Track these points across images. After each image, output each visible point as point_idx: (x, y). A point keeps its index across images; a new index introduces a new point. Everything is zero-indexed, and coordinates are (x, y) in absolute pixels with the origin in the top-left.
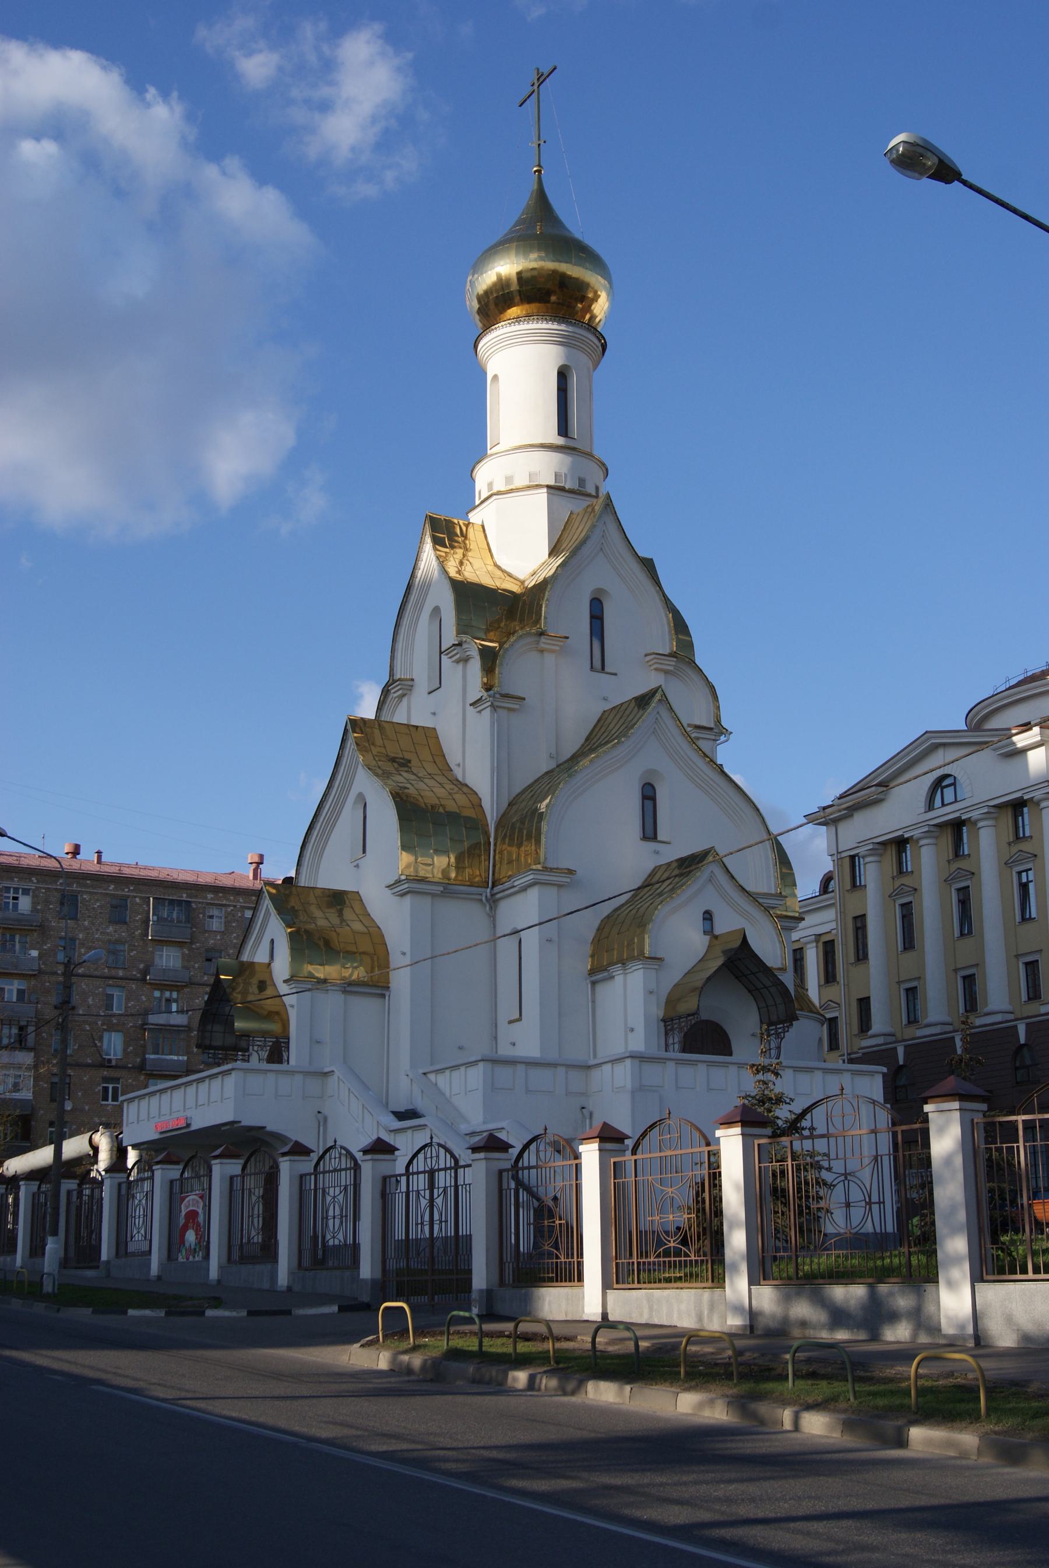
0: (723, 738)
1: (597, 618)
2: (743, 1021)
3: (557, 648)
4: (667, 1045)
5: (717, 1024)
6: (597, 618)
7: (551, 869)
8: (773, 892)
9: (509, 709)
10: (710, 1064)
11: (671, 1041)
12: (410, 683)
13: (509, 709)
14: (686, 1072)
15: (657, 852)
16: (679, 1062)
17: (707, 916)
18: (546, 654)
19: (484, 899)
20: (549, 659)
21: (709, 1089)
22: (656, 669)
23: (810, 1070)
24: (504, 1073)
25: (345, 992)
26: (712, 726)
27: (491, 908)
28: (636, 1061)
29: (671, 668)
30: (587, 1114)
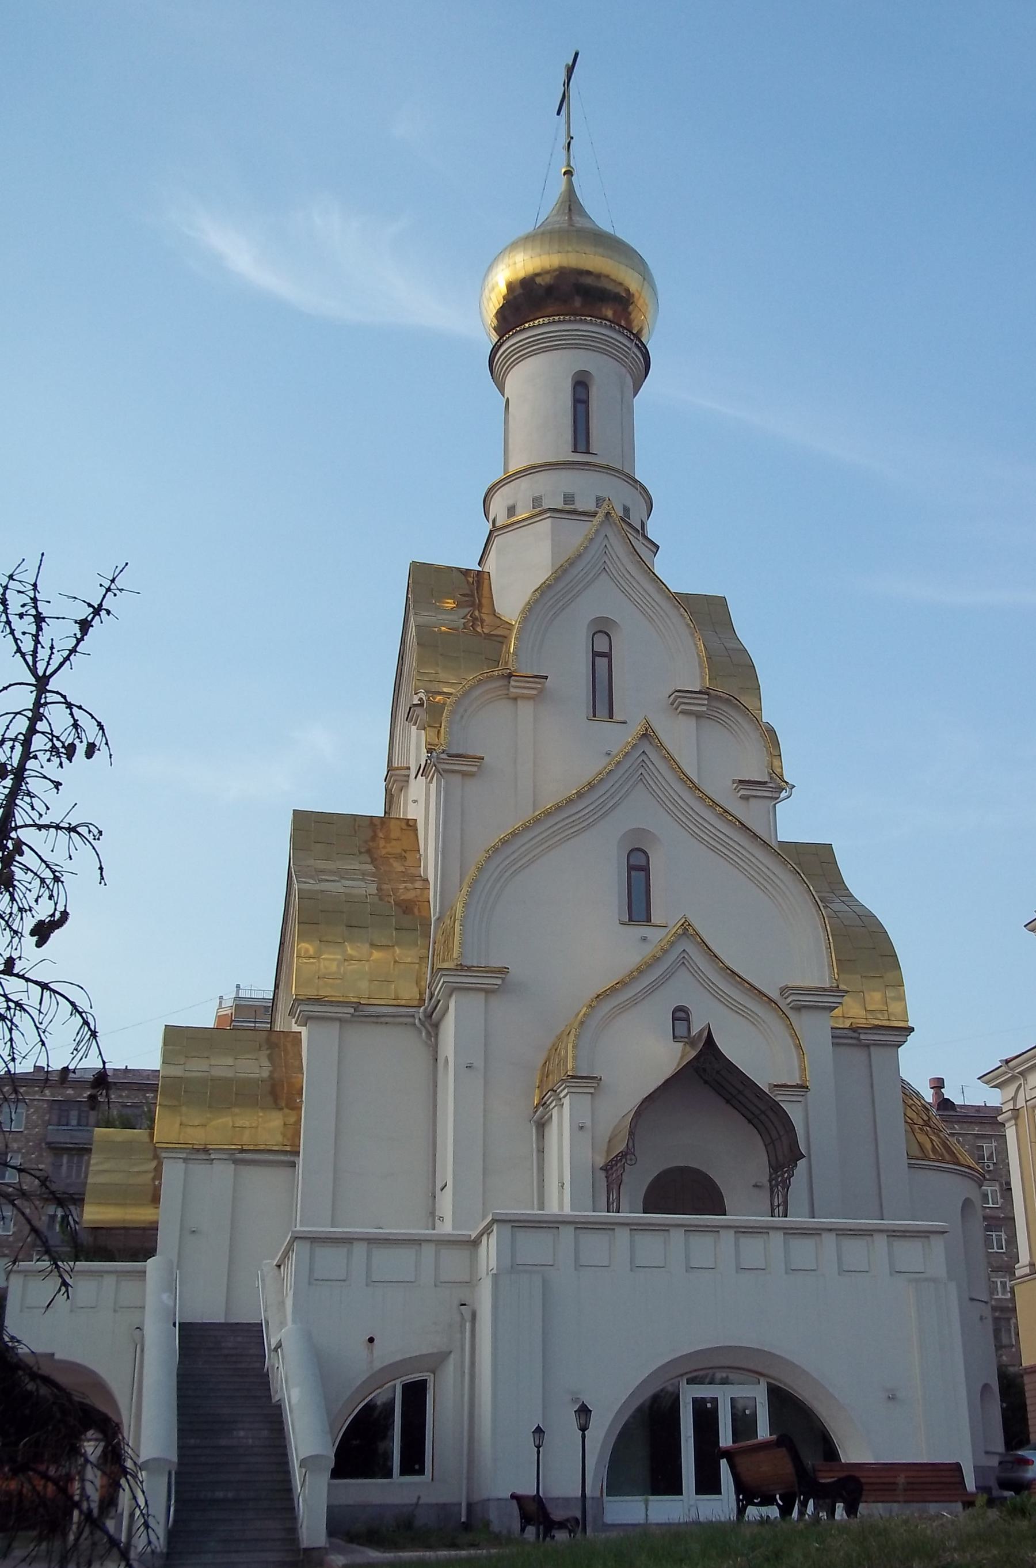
0: (783, 794)
1: (601, 657)
2: (734, 1160)
3: (534, 692)
4: (773, 1211)
5: (697, 1172)
6: (601, 657)
7: (469, 968)
8: (827, 985)
9: (465, 774)
10: (690, 1230)
11: (28, 1178)
12: (405, 772)
13: (465, 774)
14: (650, 1246)
15: (644, 939)
16: (635, 1227)
17: (682, 1015)
18: (519, 702)
19: (417, 1021)
20: (525, 708)
21: (690, 1269)
22: (683, 712)
23: (867, 1233)
24: (331, 1259)
25: (236, 1162)
26: (766, 779)
27: (428, 1033)
28: (508, 1227)
29: (704, 709)
30: (468, 1316)
